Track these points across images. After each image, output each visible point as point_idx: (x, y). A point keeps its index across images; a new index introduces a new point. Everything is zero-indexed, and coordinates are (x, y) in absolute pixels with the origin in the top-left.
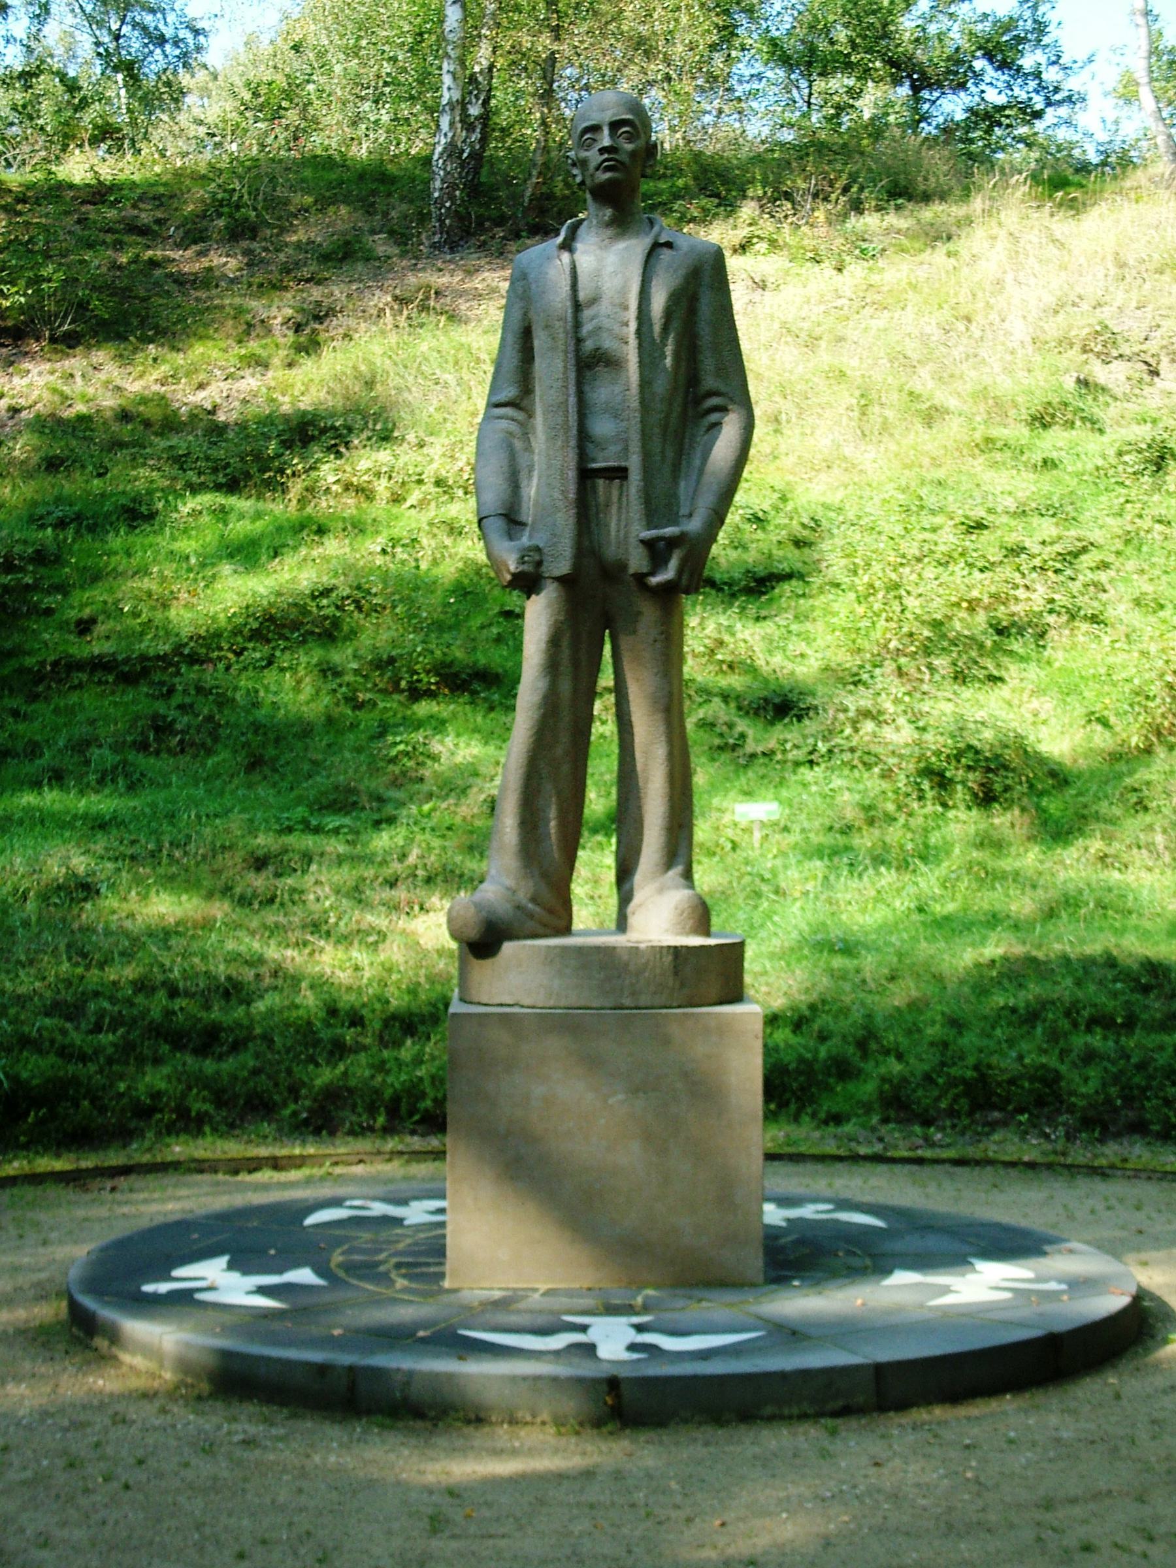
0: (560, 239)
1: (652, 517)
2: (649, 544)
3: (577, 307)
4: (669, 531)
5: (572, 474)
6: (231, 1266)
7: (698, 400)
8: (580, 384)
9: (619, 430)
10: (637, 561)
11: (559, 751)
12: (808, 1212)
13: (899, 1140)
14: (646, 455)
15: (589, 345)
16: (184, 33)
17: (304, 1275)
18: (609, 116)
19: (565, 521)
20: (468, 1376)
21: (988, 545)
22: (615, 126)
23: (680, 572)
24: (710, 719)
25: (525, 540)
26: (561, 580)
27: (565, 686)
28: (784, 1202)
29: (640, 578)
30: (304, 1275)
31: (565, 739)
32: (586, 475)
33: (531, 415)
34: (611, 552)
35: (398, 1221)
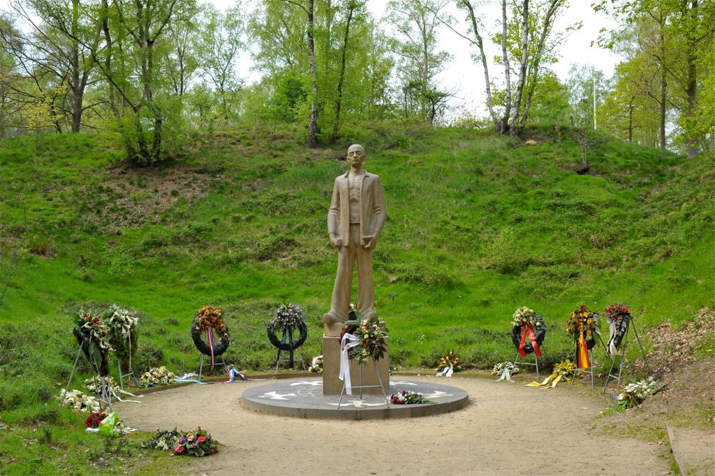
0: (345, 175)
1: (365, 233)
2: (364, 239)
3: (349, 189)
4: (369, 236)
5: (348, 225)
6: (276, 393)
7: (374, 209)
8: (349, 205)
9: (359, 214)
10: (362, 242)
11: (346, 282)
12: (401, 383)
13: (422, 370)
14: (364, 220)
15: (352, 198)
16: (119, 106)
17: (293, 395)
18: (356, 150)
19: (347, 235)
20: (547, 377)
21: (661, 251)
22: (357, 152)
23: (371, 245)
24: (507, 276)
25: (339, 238)
26: (347, 247)
27: (347, 269)
28: (394, 381)
29: (363, 246)
30: (293, 395)
31: (347, 280)
32: (351, 225)
33: (339, 211)
34: (356, 241)
35: (311, 385)
